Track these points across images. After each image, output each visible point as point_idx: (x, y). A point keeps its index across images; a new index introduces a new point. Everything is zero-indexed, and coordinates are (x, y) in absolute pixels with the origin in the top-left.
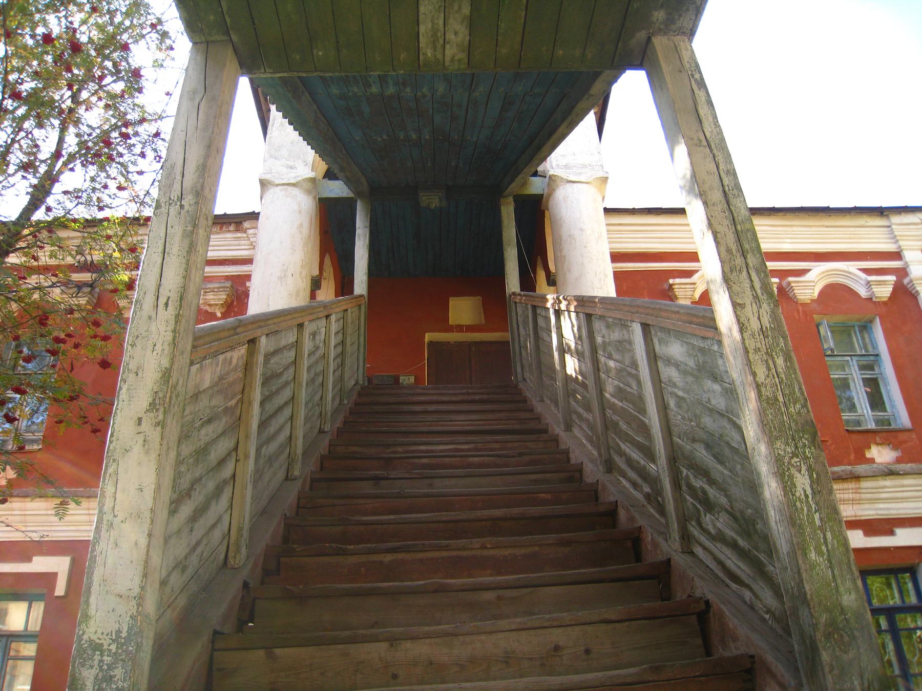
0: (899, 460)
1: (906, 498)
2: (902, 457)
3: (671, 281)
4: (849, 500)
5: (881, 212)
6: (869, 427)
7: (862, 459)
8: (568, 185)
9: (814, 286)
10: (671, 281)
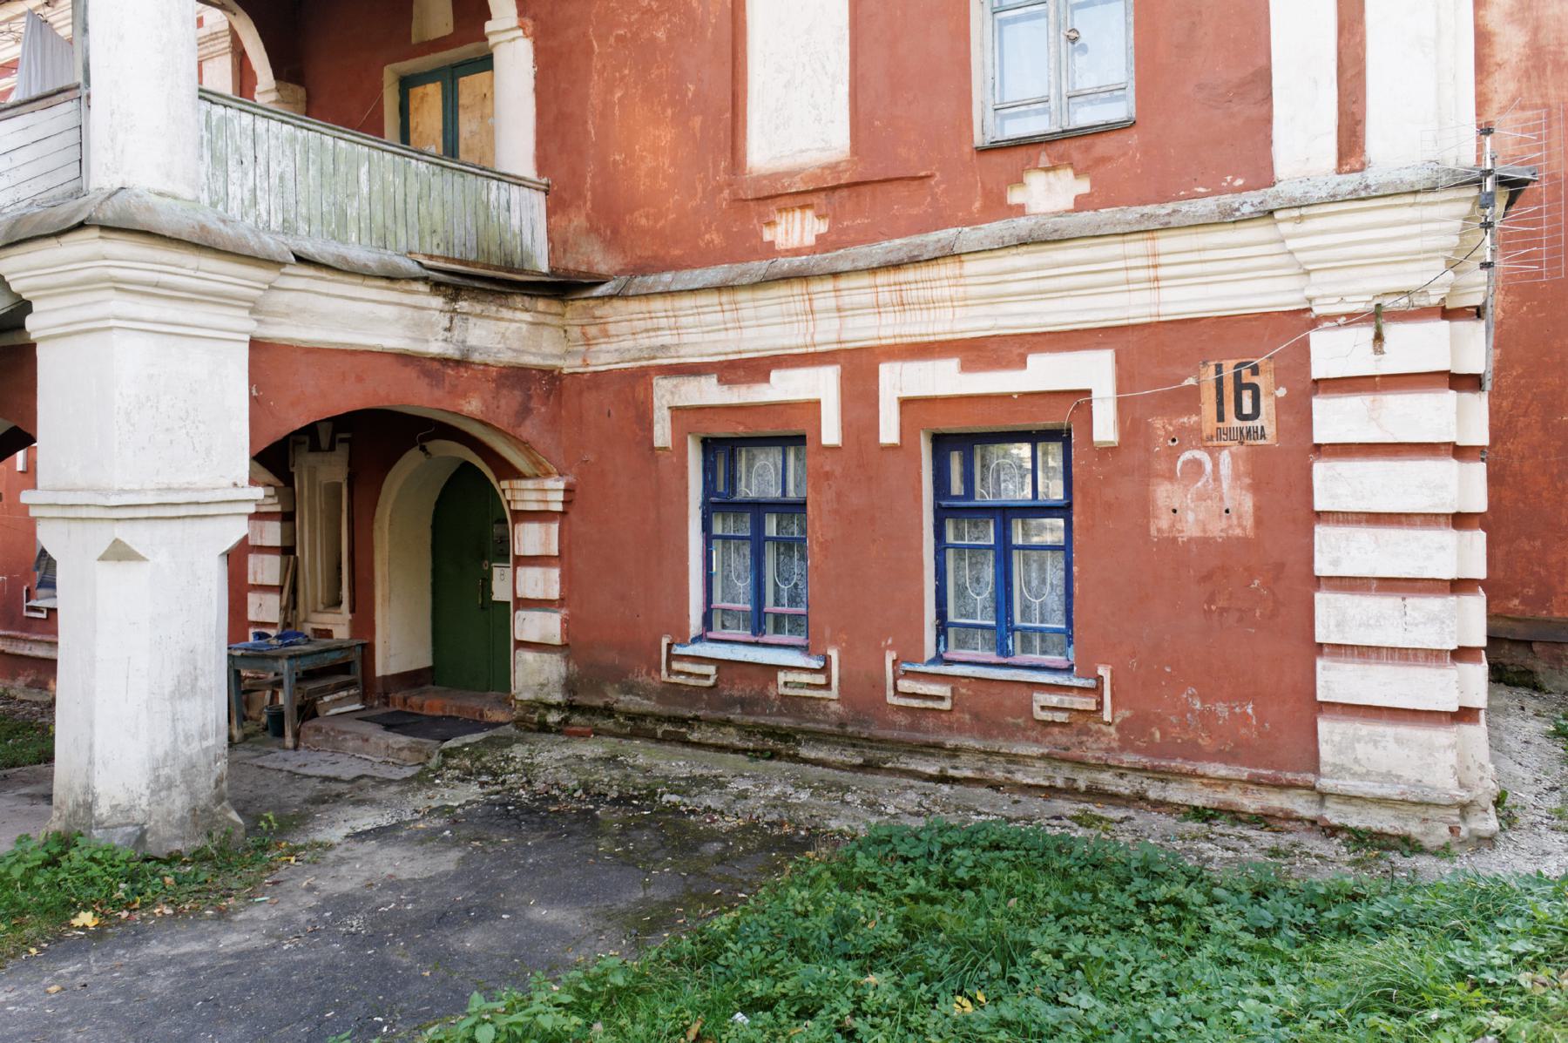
7: (997, 207)
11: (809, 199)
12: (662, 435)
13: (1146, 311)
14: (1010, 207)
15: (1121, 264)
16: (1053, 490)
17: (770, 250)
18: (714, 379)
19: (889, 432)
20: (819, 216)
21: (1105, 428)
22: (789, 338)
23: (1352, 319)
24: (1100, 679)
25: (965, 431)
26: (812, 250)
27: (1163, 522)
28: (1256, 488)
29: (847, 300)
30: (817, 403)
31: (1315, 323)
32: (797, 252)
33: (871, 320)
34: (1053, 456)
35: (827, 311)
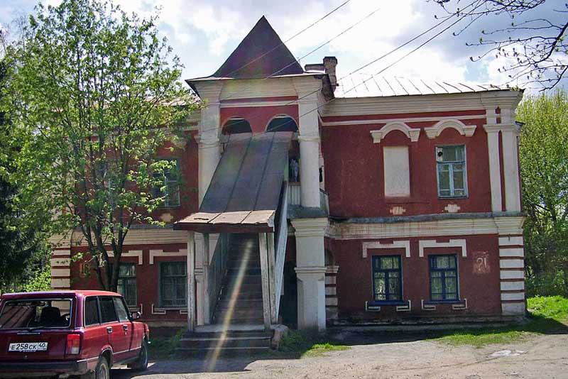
12: (365, 255)
16: (396, 267)
17: (392, 215)
18: (435, 241)
19: (421, 255)
20: (458, 206)
21: (464, 254)
27: (475, 271)
28: (490, 265)
29: (412, 227)
30: (461, 247)
32: (399, 216)
34: (396, 260)
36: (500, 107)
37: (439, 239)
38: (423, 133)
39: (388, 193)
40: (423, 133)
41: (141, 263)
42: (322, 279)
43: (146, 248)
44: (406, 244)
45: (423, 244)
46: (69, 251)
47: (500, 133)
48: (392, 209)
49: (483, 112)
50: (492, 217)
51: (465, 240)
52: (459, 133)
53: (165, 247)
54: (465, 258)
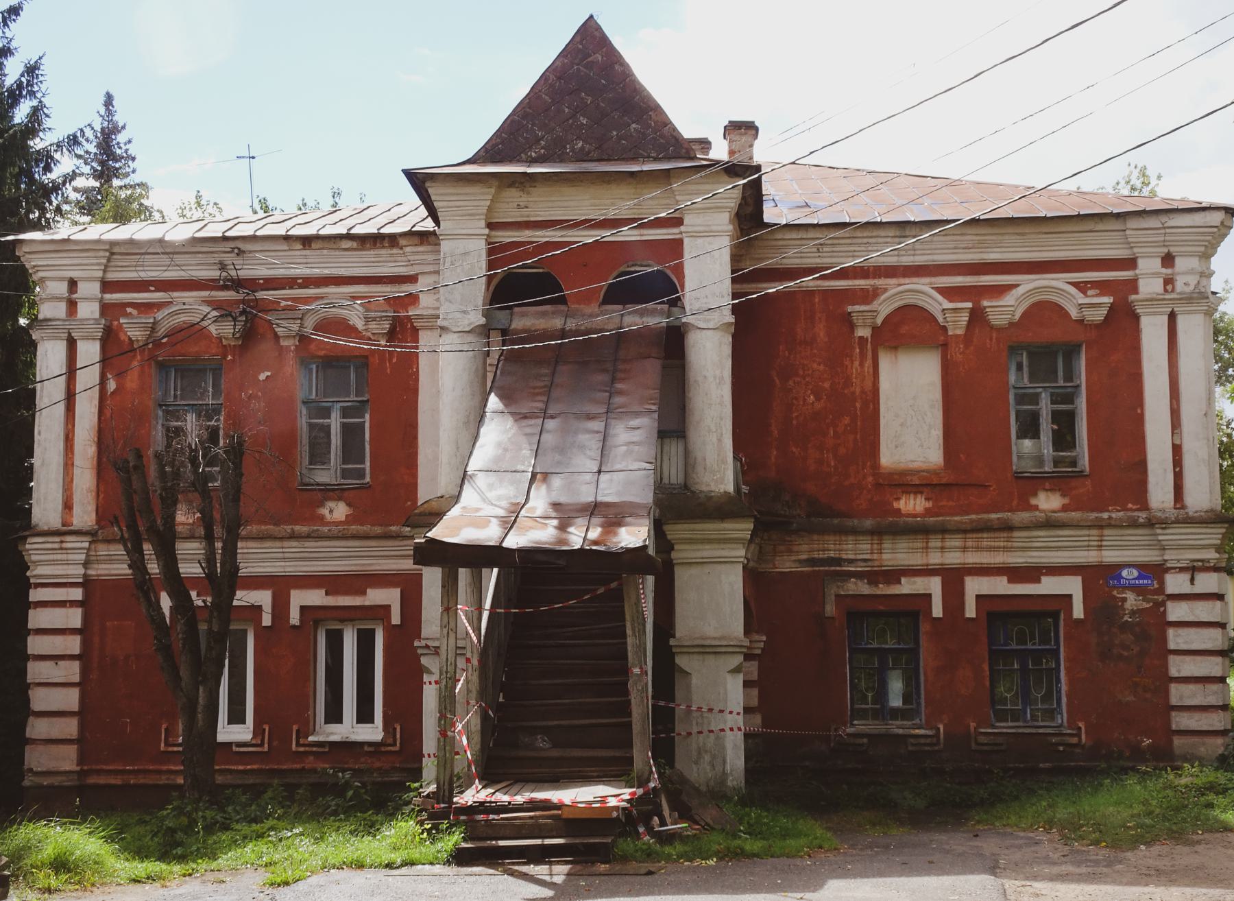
0: (1065, 508)
1: (1060, 547)
2: (1069, 504)
3: (850, 309)
4: (1000, 548)
5: (1118, 216)
6: (1047, 469)
8: (698, 331)
9: (1014, 312)
10: (850, 309)
11: (921, 489)
12: (830, 609)
13: (1096, 560)
14: (1032, 506)
15: (1087, 538)
18: (1005, 579)
19: (971, 611)
20: (927, 499)
22: (917, 560)
23: (1182, 570)
24: (1080, 728)
25: (68, 710)
26: (922, 515)
31: (1168, 570)
33: (958, 554)
35: (936, 548)
36: (1172, 249)
37: (1016, 574)
38: (977, 316)
39: (890, 457)
40: (977, 316)
41: (267, 620)
42: (736, 670)
43: (281, 586)
44: (934, 586)
45: (975, 587)
46: (1172, 617)
47: (1172, 317)
48: (898, 499)
49: (1131, 263)
50: (1150, 524)
51: (1079, 579)
52: (1067, 315)
53: (332, 583)
54: (1078, 621)
